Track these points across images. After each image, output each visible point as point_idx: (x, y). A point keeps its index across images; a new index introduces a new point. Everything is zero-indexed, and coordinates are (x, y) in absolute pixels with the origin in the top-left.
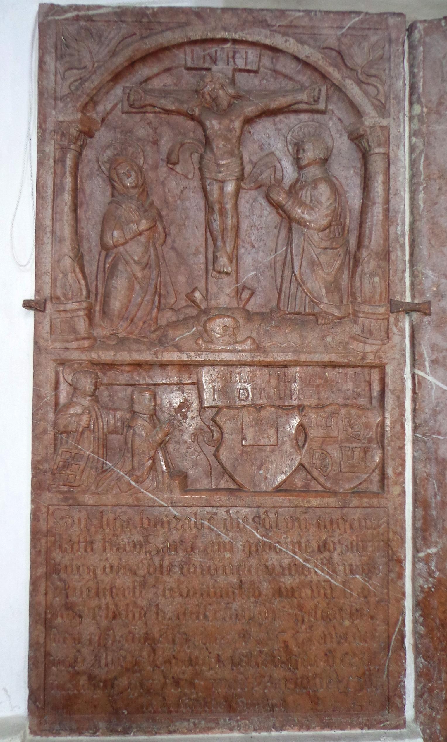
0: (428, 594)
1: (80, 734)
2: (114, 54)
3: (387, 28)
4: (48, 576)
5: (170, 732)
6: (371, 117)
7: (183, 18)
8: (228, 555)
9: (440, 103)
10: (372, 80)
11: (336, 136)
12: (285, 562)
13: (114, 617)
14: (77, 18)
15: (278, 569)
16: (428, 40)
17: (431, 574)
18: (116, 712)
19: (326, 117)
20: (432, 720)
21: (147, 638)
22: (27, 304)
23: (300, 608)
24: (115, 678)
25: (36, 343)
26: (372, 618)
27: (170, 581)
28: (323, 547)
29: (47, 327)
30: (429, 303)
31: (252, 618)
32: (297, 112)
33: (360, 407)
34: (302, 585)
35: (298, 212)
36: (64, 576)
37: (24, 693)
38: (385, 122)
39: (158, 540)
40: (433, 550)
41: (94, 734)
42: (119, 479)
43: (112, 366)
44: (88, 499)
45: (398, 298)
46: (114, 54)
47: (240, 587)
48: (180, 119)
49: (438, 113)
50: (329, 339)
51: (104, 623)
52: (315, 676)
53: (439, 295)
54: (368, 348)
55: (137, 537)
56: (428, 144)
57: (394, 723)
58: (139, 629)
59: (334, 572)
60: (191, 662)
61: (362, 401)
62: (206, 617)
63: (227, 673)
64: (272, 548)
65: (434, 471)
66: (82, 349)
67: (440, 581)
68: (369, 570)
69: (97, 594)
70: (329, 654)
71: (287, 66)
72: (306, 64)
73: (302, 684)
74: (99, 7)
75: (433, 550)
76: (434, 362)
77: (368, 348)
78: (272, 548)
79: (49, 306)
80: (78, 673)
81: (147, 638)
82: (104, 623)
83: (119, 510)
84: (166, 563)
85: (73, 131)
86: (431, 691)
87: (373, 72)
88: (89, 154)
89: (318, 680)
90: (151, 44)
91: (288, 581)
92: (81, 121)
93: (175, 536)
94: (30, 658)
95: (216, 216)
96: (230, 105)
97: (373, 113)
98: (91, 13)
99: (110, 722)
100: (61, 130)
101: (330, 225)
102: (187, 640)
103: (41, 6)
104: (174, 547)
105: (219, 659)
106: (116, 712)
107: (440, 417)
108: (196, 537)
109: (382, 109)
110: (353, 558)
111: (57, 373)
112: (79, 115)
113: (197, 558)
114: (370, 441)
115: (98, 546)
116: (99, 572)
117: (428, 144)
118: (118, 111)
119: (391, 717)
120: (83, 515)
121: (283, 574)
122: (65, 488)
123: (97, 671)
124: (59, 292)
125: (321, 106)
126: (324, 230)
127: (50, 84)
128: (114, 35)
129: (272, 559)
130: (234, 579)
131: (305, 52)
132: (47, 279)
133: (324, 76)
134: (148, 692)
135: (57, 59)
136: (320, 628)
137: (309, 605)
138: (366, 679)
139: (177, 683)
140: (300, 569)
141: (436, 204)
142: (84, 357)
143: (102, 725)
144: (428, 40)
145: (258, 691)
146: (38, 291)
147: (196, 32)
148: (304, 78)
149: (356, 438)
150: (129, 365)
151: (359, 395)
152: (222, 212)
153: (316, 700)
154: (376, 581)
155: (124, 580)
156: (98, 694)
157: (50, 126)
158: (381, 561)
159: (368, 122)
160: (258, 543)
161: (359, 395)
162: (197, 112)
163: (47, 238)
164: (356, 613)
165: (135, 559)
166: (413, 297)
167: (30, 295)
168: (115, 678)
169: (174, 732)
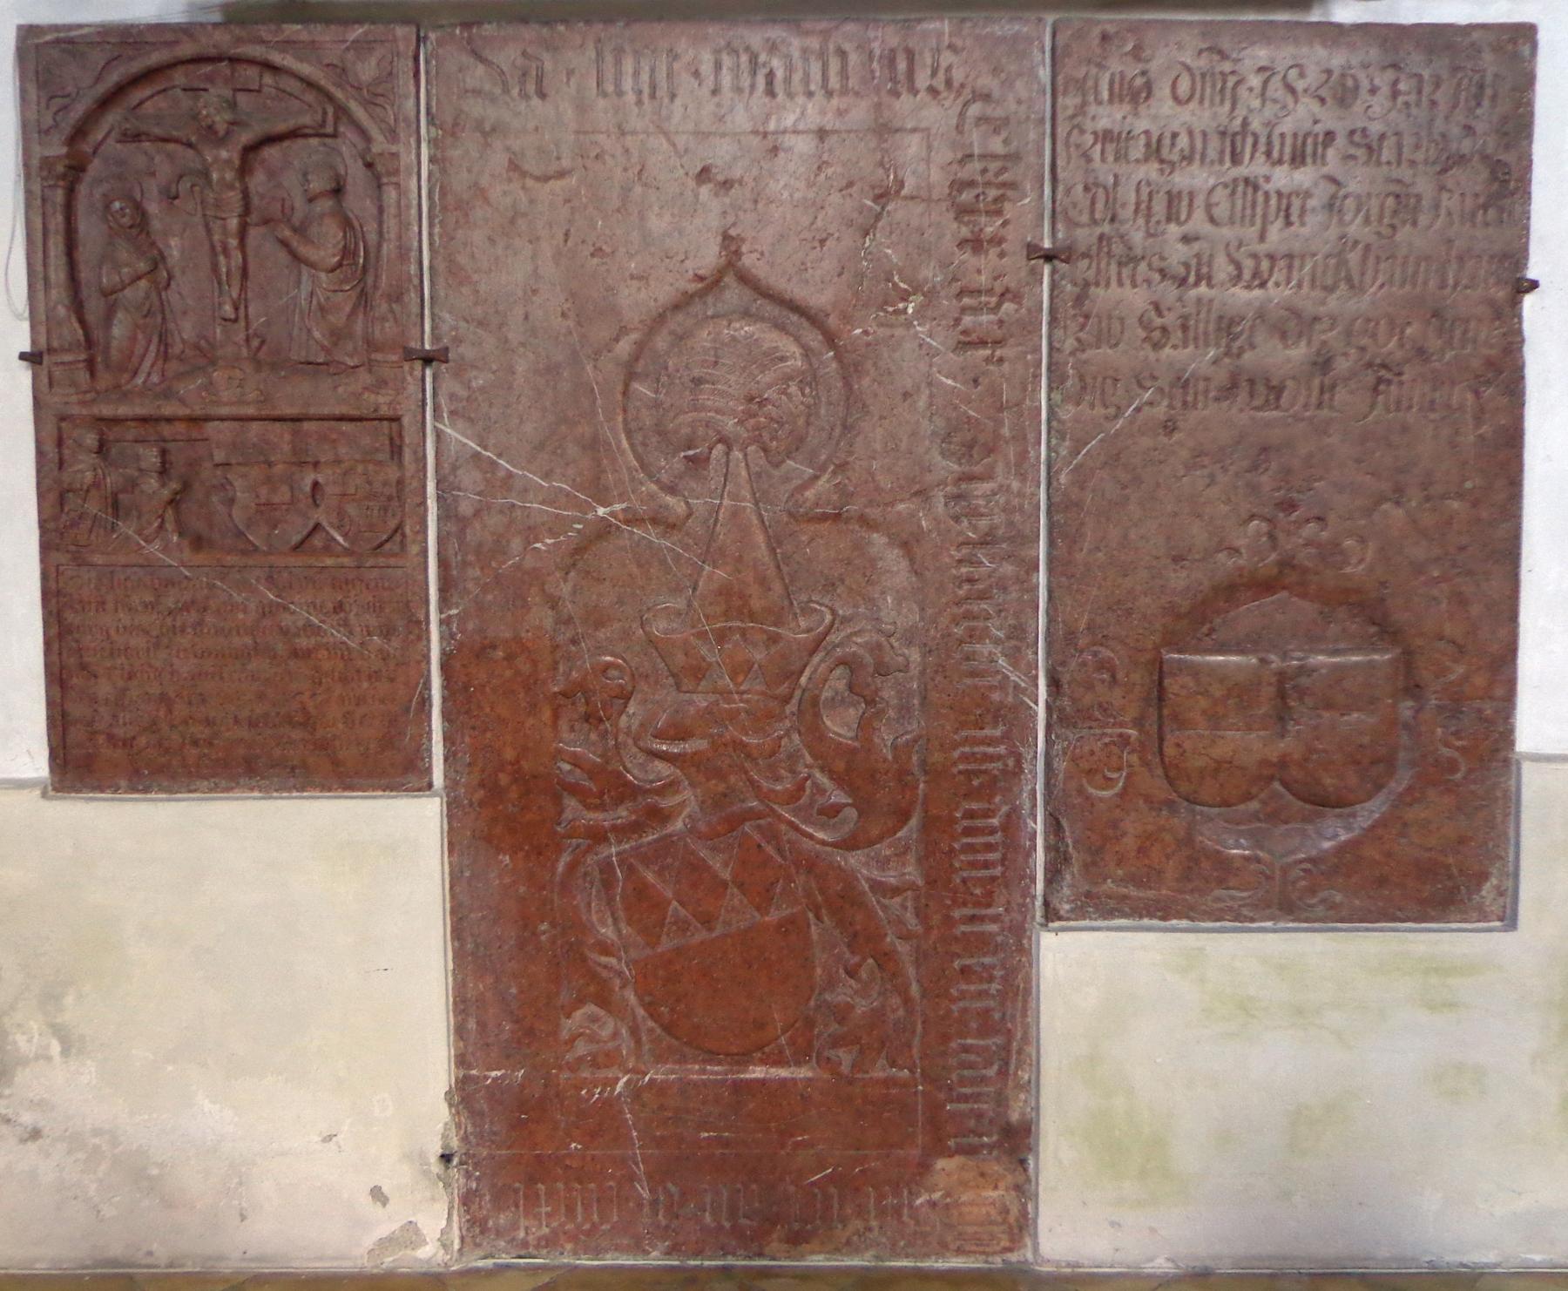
0: (482, 651)
1: (102, 791)
2: (98, 79)
3: (395, 40)
4: (60, 636)
5: (190, 791)
6: (380, 144)
7: (169, 37)
8: (241, 616)
9: (456, 124)
10: (380, 100)
11: (349, 161)
12: (300, 623)
13: (130, 678)
14: (58, 41)
15: (293, 630)
16: (440, 51)
17: (452, 636)
18: (137, 772)
19: (339, 140)
20: (456, 783)
21: (163, 697)
22: (23, 356)
23: (317, 669)
24: (134, 738)
25: (35, 398)
26: (392, 680)
27: (184, 641)
28: (339, 608)
29: (46, 380)
30: (446, 349)
31: (267, 679)
32: (306, 136)
33: (380, 463)
34: (318, 647)
35: (304, 250)
36: (76, 636)
37: (46, 753)
38: (394, 149)
39: (169, 602)
40: (454, 612)
41: (115, 792)
42: (128, 538)
43: (116, 421)
44: (98, 559)
45: (413, 345)
46: (98, 79)
47: (255, 649)
48: (179, 148)
49: (453, 134)
50: (340, 390)
51: (121, 684)
52: (335, 737)
53: (458, 340)
54: (381, 399)
55: (149, 598)
56: (443, 171)
57: (417, 786)
58: (155, 690)
59: (351, 633)
60: (208, 722)
61: (380, 456)
62: (222, 678)
63: (243, 733)
64: (286, 608)
65: (454, 529)
66: (83, 403)
67: (461, 645)
68: (387, 632)
69: (112, 654)
70: (347, 716)
71: (293, 85)
72: (310, 84)
73: (323, 746)
74: (80, 26)
75: (454, 612)
76: (452, 413)
77: (381, 399)
78: (286, 608)
79: (46, 358)
80: (95, 733)
81: (163, 697)
82: (121, 684)
83: (129, 571)
84: (178, 624)
85: (60, 169)
86: (455, 754)
87: (380, 90)
88: (83, 189)
89: (337, 743)
90: (137, 66)
91: (303, 642)
92: (67, 156)
93: (187, 597)
94: (48, 718)
95: (222, 258)
96: (228, 133)
97: (380, 138)
98: (73, 34)
99: (130, 780)
100: (47, 163)
101: (340, 265)
102: (204, 701)
103: (20, 28)
104: (186, 608)
105: (236, 721)
106: (137, 772)
107: (460, 472)
108: (207, 598)
109: (392, 135)
110: (373, 621)
111: (59, 429)
112: (64, 150)
113: (210, 619)
114: (390, 498)
115: (110, 606)
116: (112, 632)
117: (443, 171)
118: (110, 141)
119: (413, 780)
120: (93, 574)
121: (299, 636)
122: (73, 548)
123: (116, 731)
124: (55, 344)
125: (329, 129)
126: (333, 270)
127: (32, 116)
128: (98, 58)
129: (286, 620)
130: (248, 640)
131: (305, 69)
132: (43, 329)
133: (330, 98)
134: (167, 751)
135: (39, 88)
136: (338, 690)
137: (327, 666)
138: (387, 742)
139: (195, 743)
140: (317, 631)
141: (453, 239)
142: (84, 412)
143: (123, 783)
144: (440, 51)
145: (277, 752)
146: (34, 342)
147: (187, 49)
148: (310, 97)
149: (372, 496)
150: (133, 420)
151: (377, 450)
152: (226, 251)
153: (336, 763)
154: (395, 643)
155: (138, 642)
156: (119, 754)
157: (35, 162)
158: (400, 624)
159: (375, 149)
160: (271, 602)
161: (377, 450)
162: (193, 139)
163: (40, 286)
164: (374, 676)
165: (145, 619)
166: (432, 344)
167: (27, 348)
168: (134, 738)
169: (195, 791)
